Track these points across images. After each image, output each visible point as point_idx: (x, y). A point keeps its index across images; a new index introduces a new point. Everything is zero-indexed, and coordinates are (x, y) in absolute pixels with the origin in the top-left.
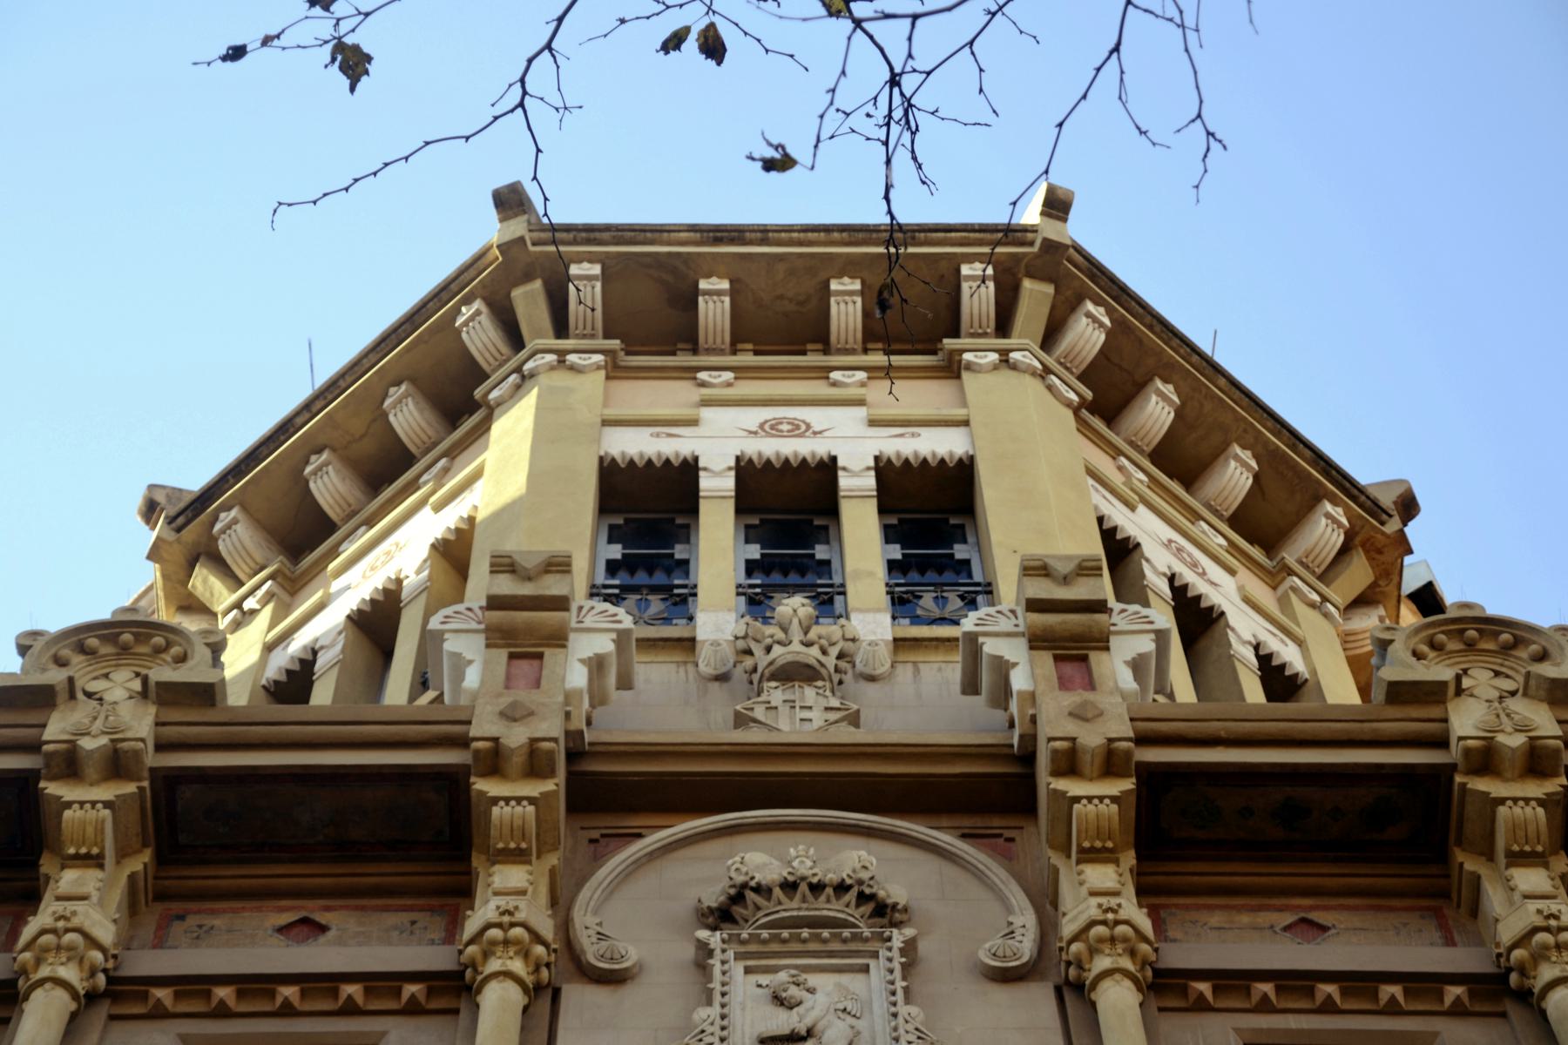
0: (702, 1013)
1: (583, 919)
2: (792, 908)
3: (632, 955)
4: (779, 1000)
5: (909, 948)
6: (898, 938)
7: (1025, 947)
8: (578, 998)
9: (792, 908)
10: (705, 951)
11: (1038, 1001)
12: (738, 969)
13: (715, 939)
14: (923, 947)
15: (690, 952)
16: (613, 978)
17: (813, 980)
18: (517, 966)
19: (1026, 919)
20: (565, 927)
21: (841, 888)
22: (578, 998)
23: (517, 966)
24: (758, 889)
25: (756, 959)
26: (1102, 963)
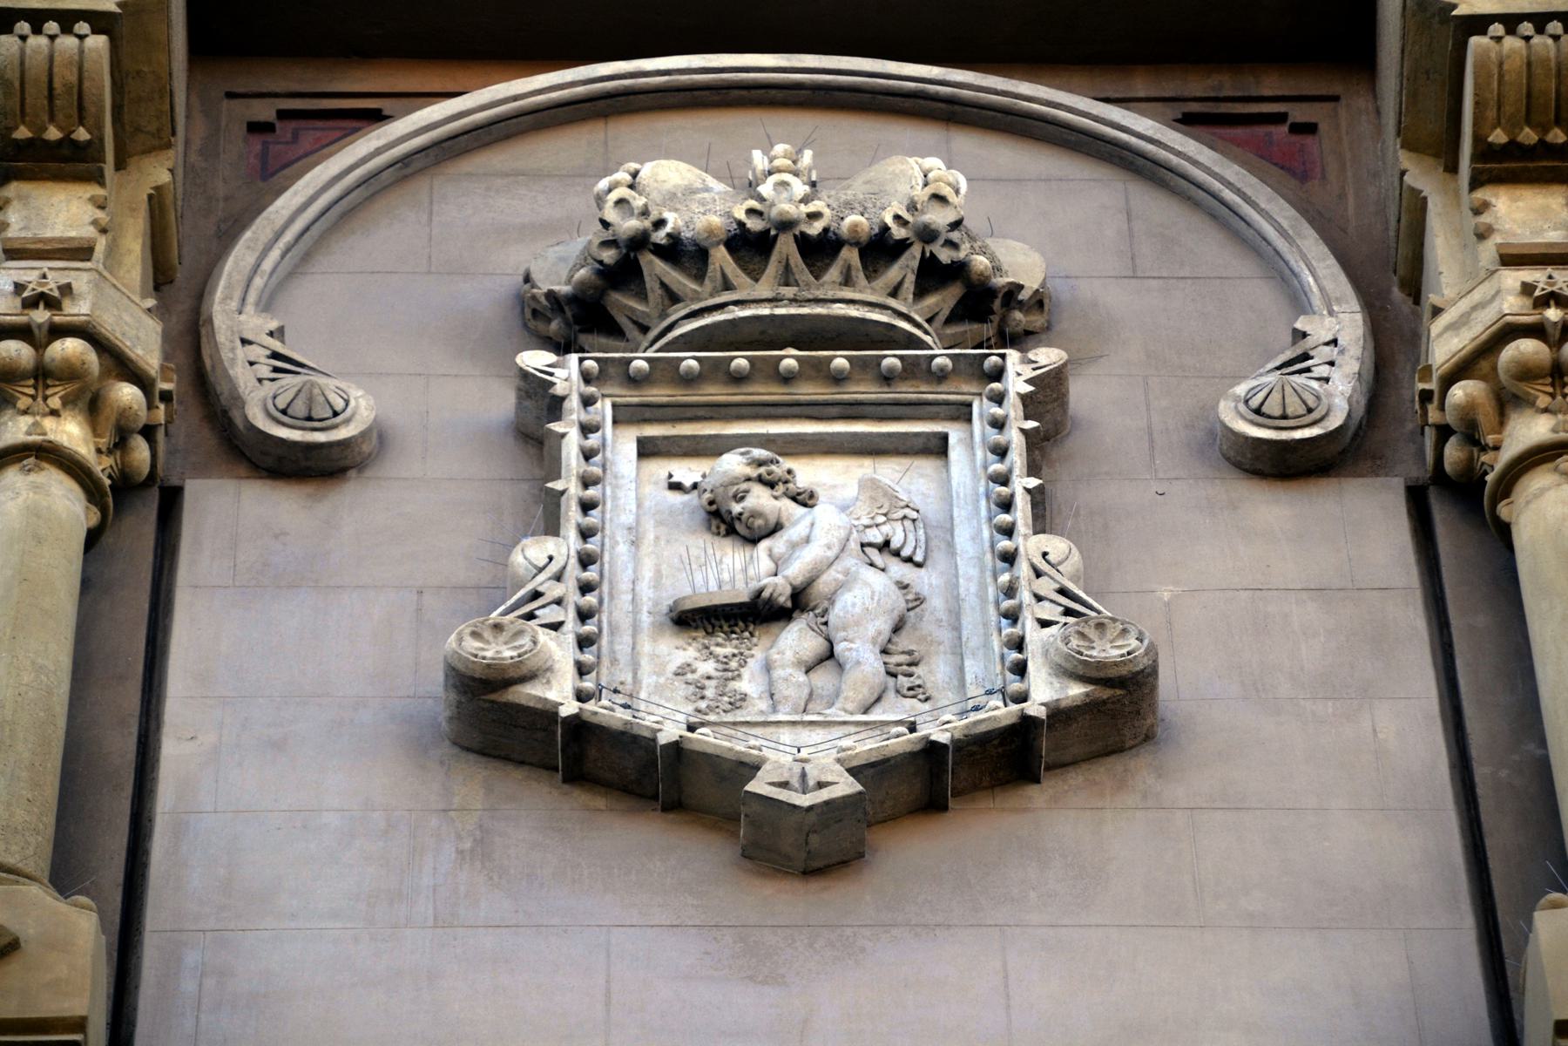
0: (535, 551)
1: (238, 321)
2: (758, 297)
3: (362, 410)
4: (725, 522)
5: (1047, 396)
6: (1018, 373)
7: (1338, 391)
8: (227, 517)
9: (758, 297)
10: (541, 401)
11: (1364, 527)
12: (622, 447)
13: (567, 374)
14: (1081, 394)
15: (502, 403)
16: (315, 466)
17: (807, 473)
18: (71, 432)
19: (1339, 323)
20: (191, 339)
21: (879, 249)
22: (227, 517)
23: (71, 432)
24: (679, 251)
25: (668, 420)
26: (1531, 429)
